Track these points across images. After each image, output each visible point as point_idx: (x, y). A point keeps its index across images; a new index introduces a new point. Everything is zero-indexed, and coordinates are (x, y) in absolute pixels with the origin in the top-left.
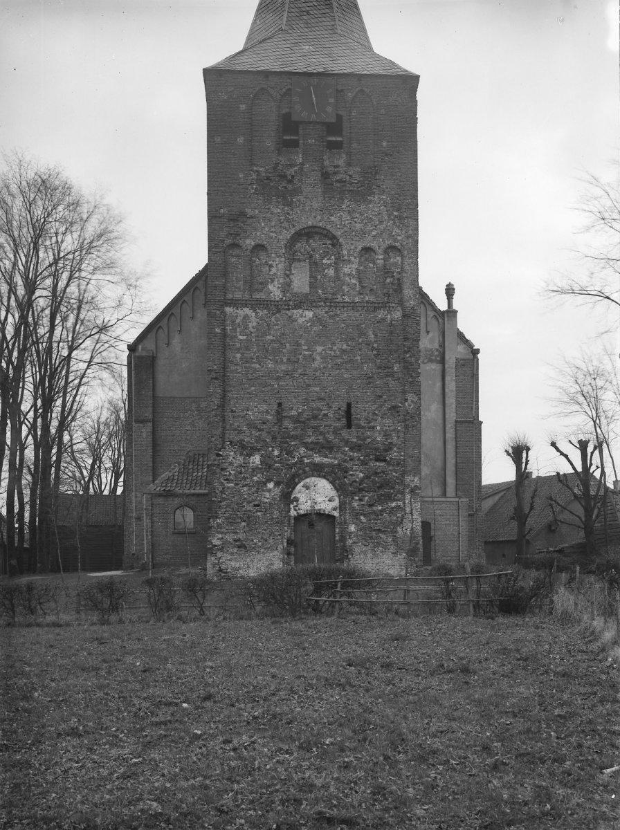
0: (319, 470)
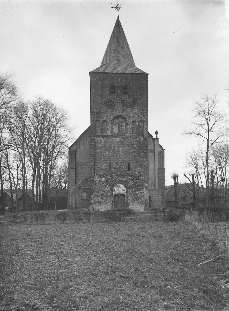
0: (121, 182)
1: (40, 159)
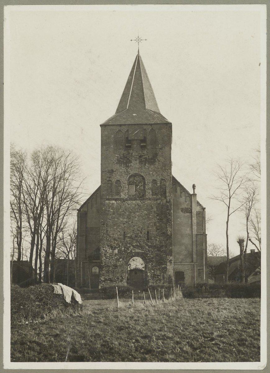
0: (137, 255)
1: (42, 215)
